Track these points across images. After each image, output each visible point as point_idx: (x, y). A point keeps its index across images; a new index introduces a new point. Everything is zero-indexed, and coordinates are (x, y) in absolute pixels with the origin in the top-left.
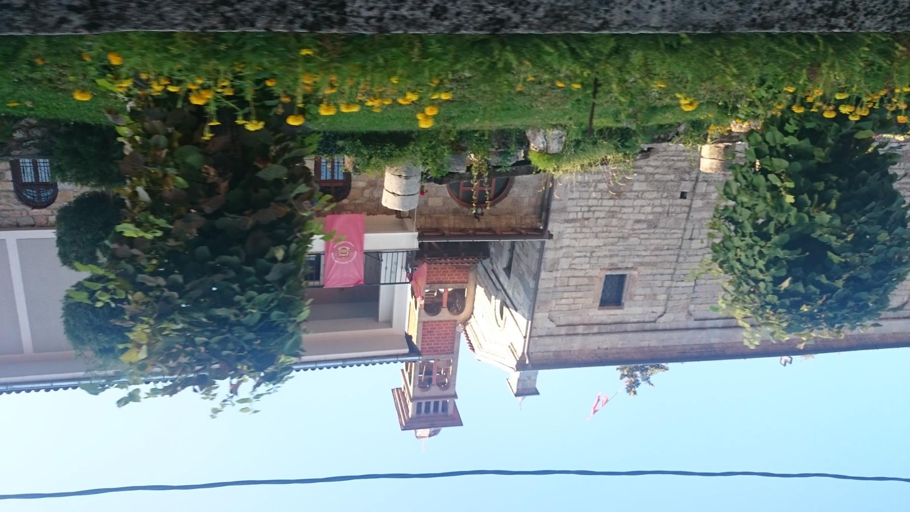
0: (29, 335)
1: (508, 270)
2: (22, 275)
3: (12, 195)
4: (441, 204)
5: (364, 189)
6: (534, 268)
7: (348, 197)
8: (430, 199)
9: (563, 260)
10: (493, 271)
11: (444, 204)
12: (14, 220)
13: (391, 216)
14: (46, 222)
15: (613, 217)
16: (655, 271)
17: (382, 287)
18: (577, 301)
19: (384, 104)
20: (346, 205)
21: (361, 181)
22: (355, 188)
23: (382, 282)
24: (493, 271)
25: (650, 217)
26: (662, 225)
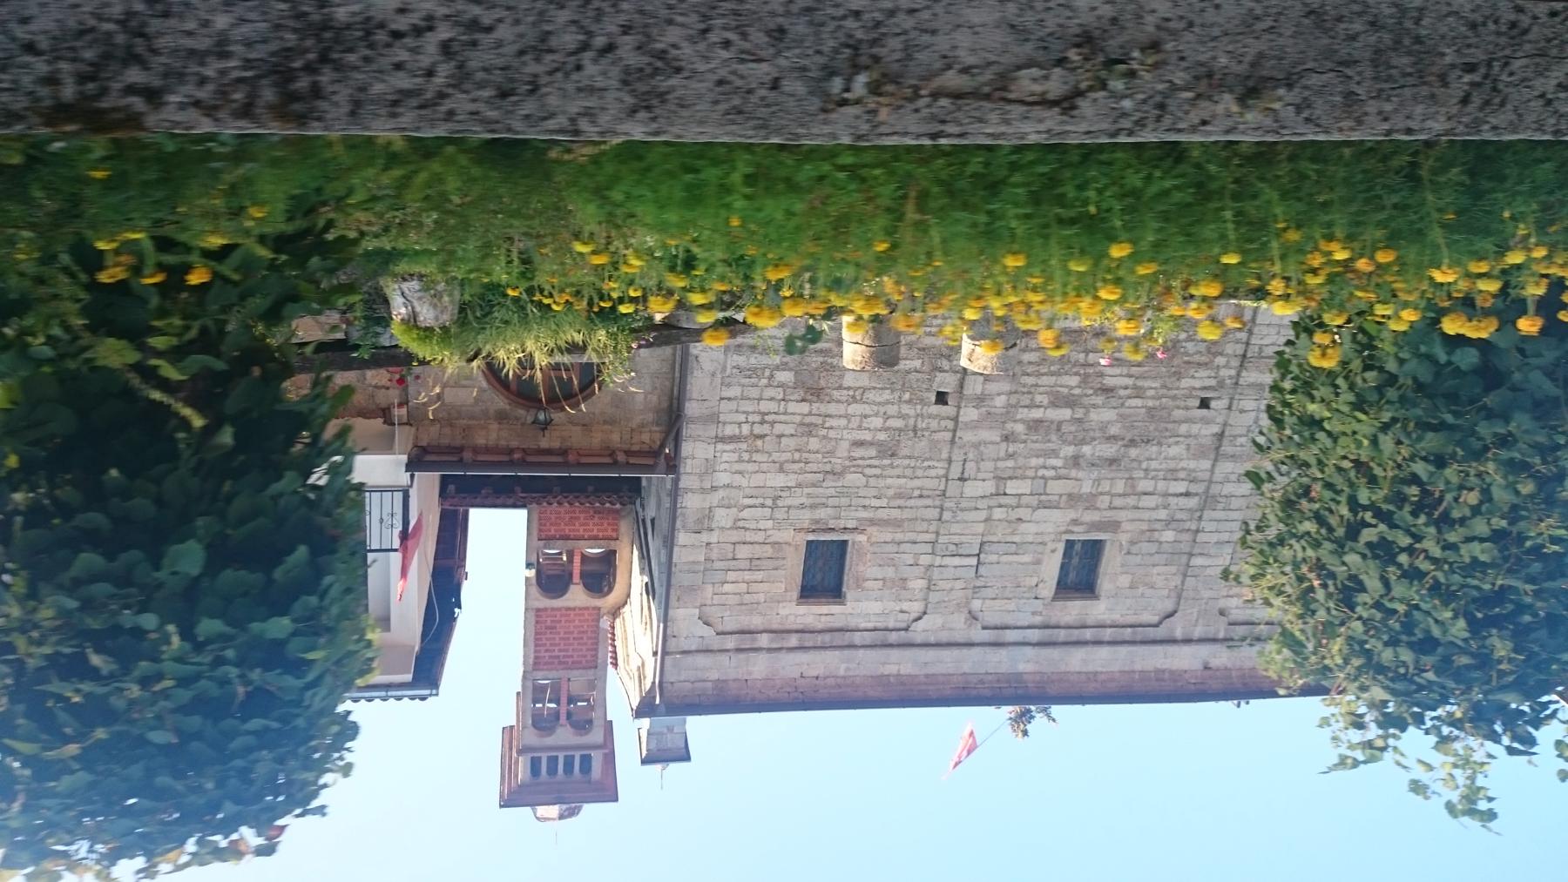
25: (882, 436)
26: (905, 452)
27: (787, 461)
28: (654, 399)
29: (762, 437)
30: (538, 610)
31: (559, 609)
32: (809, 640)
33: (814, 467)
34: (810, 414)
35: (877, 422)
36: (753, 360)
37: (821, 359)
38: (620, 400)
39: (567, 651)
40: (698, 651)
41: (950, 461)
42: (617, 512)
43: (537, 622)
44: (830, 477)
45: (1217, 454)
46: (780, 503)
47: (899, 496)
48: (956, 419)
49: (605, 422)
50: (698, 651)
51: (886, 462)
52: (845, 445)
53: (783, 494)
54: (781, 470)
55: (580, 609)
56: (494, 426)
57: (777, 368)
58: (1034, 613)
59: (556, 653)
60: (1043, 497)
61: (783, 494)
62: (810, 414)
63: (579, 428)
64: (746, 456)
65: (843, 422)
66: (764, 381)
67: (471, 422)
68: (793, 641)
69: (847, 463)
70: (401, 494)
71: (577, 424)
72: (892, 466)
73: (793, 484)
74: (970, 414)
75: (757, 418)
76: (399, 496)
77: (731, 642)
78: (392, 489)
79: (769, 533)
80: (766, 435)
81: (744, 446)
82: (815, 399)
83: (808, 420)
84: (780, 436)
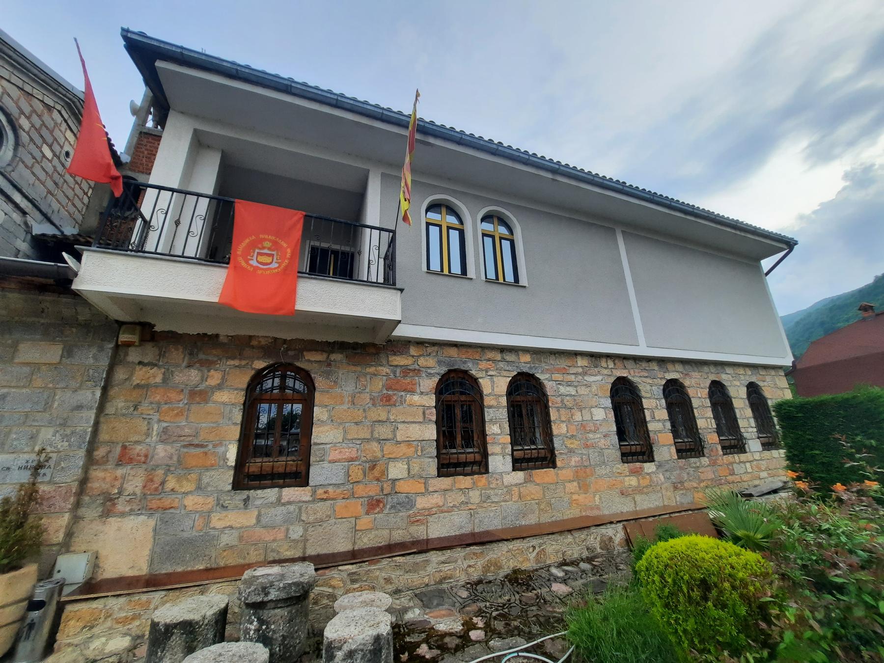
0: (620, 246)
2: (60, 76)
3: (643, 394)
4: (22, 347)
5: (220, 387)
7: (253, 372)
8: (56, 359)
10: (24, 213)
11: (15, 346)
12: (638, 366)
13: (167, 328)
14: (616, 361)
17: (210, 192)
19: (251, 631)
20: (258, 358)
21: (224, 404)
22: (242, 390)
23: (204, 203)
24: (24, 213)
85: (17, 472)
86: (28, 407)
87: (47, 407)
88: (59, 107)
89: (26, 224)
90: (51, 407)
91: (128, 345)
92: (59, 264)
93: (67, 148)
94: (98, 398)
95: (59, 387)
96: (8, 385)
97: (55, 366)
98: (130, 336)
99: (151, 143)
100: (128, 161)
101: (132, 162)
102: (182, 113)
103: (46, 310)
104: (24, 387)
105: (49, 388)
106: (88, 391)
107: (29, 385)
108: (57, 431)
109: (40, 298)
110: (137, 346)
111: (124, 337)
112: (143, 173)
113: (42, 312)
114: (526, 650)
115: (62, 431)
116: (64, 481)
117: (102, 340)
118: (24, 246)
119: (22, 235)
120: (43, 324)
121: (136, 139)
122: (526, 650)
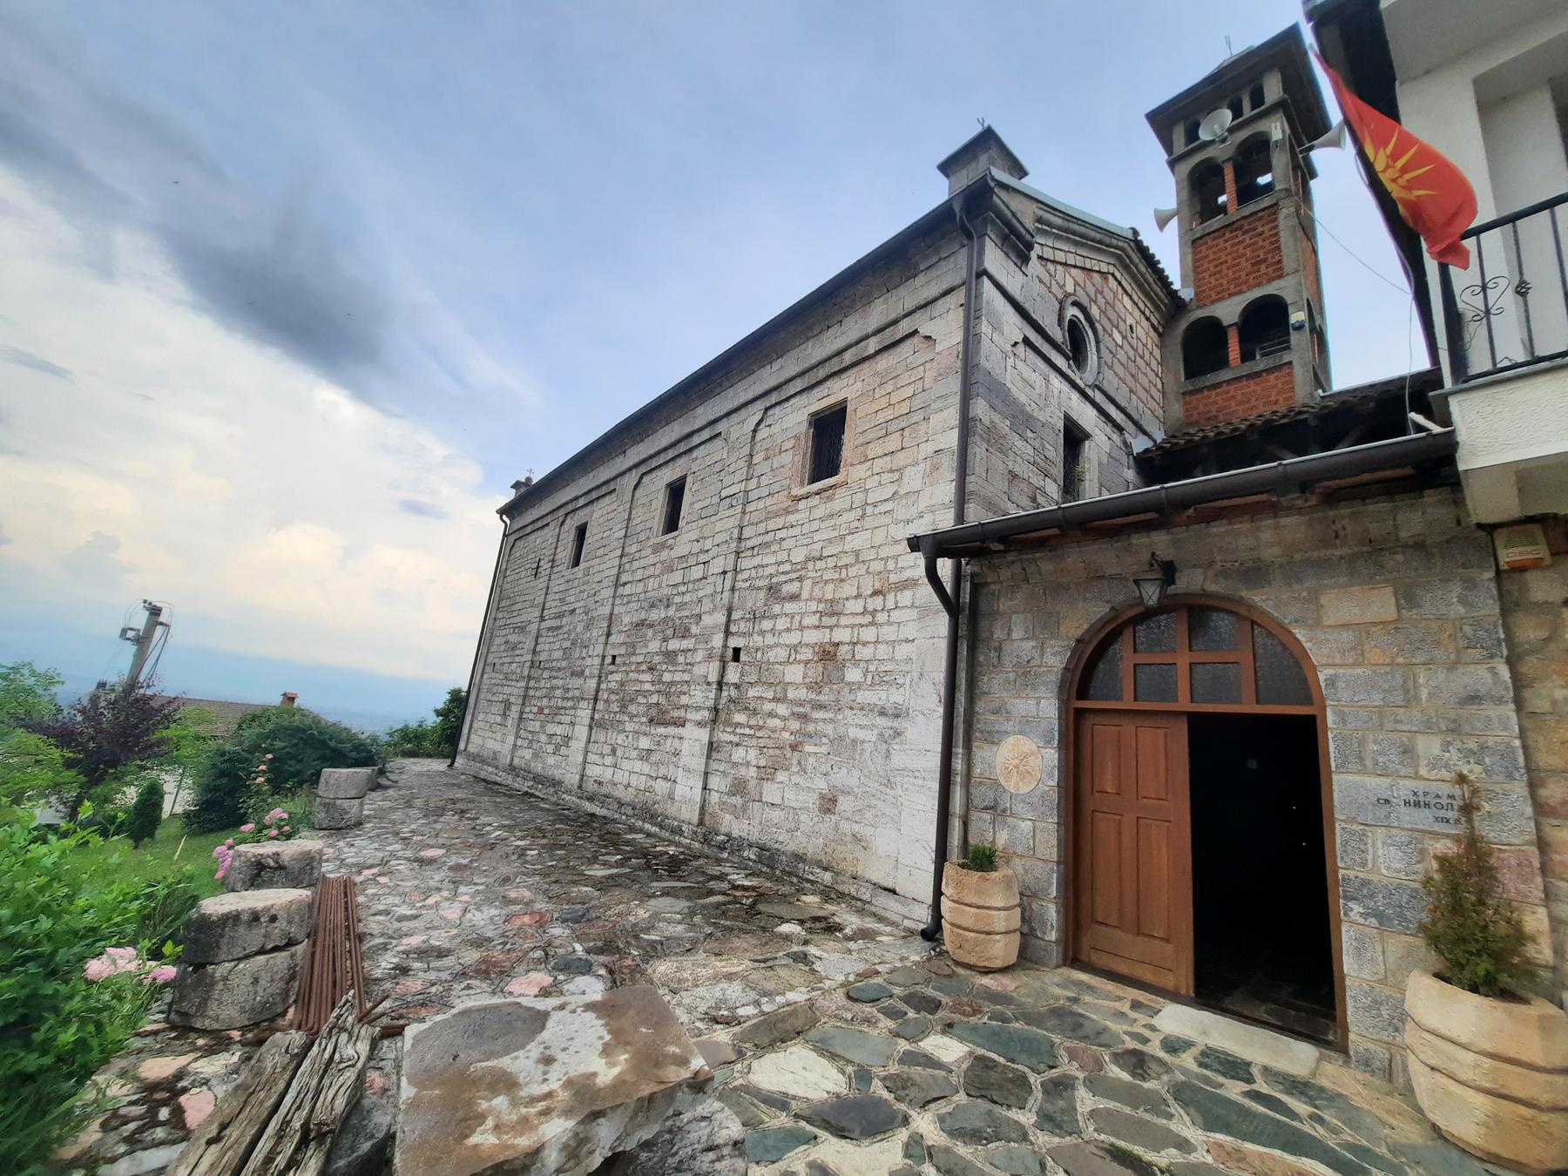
1: (1074, 437)
6: (978, 449)
9: (916, 485)
11: (1314, 598)
15: (832, 602)
16: (769, 501)
18: (883, 403)
25: (777, 609)
26: (762, 594)
27: (852, 565)
28: (998, 634)
29: (876, 593)
30: (1281, 277)
31: (1250, 288)
32: (834, 365)
33: (831, 562)
34: (831, 628)
35: (782, 624)
36: (883, 695)
37: (821, 698)
38: (1045, 625)
39: (1232, 246)
40: (935, 300)
41: (733, 589)
42: (1189, 425)
43: (1279, 262)
44: (817, 554)
45: (610, 619)
46: (859, 512)
47: (767, 545)
48: (727, 633)
49: (1066, 587)
50: (935, 300)
51: (775, 580)
52: (805, 595)
53: (856, 524)
54: (857, 553)
55: (1223, 298)
56: (1268, 554)
57: (860, 685)
58: (696, 459)
59: (1247, 237)
60: (685, 565)
61: (856, 524)
62: (831, 628)
63: (1108, 573)
64: (891, 565)
65: (806, 622)
66: (872, 668)
67: (1324, 553)
68: (848, 357)
69: (803, 573)
70: (1474, 369)
71: (1111, 577)
72: (772, 576)
73: (849, 538)
74: (718, 641)
75: (881, 617)
76: (1479, 361)
77: (904, 327)
78: (1500, 376)
79: (869, 473)
80: (871, 596)
81: (893, 578)
82: (828, 648)
83: (833, 621)
84: (858, 596)
85: (1403, 809)
86: (1377, 698)
87: (1410, 699)
88: (1112, 269)
89: (1125, 443)
90: (1417, 698)
91: (1520, 569)
92: (1166, 485)
93: (1130, 321)
94: (1509, 681)
95: (1418, 662)
96: (1330, 662)
97: (1396, 625)
98: (1529, 549)
99: (1232, 238)
100: (1192, 296)
101: (1197, 294)
102: (1428, 72)
103: (1341, 533)
104: (1354, 665)
105: (1398, 664)
106: (1479, 666)
107: (1363, 661)
108: (1449, 743)
109: (1332, 513)
110: (1549, 567)
111: (1509, 555)
112: (1219, 300)
113: (1337, 537)
114: (462, 990)
115: (1459, 745)
116: (1505, 841)
117: (1464, 566)
118: (1130, 474)
119: (1124, 459)
120: (1341, 558)
121: (1190, 257)
122: (462, 990)
